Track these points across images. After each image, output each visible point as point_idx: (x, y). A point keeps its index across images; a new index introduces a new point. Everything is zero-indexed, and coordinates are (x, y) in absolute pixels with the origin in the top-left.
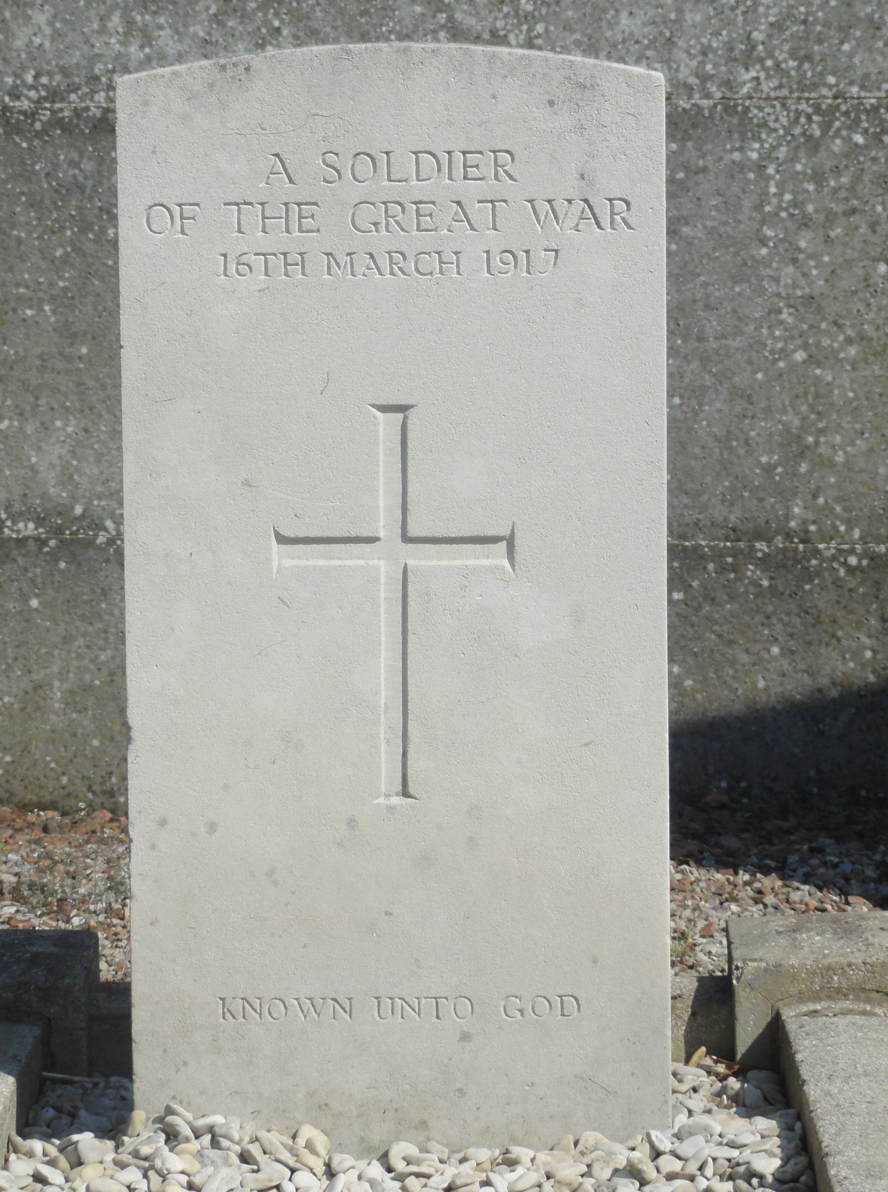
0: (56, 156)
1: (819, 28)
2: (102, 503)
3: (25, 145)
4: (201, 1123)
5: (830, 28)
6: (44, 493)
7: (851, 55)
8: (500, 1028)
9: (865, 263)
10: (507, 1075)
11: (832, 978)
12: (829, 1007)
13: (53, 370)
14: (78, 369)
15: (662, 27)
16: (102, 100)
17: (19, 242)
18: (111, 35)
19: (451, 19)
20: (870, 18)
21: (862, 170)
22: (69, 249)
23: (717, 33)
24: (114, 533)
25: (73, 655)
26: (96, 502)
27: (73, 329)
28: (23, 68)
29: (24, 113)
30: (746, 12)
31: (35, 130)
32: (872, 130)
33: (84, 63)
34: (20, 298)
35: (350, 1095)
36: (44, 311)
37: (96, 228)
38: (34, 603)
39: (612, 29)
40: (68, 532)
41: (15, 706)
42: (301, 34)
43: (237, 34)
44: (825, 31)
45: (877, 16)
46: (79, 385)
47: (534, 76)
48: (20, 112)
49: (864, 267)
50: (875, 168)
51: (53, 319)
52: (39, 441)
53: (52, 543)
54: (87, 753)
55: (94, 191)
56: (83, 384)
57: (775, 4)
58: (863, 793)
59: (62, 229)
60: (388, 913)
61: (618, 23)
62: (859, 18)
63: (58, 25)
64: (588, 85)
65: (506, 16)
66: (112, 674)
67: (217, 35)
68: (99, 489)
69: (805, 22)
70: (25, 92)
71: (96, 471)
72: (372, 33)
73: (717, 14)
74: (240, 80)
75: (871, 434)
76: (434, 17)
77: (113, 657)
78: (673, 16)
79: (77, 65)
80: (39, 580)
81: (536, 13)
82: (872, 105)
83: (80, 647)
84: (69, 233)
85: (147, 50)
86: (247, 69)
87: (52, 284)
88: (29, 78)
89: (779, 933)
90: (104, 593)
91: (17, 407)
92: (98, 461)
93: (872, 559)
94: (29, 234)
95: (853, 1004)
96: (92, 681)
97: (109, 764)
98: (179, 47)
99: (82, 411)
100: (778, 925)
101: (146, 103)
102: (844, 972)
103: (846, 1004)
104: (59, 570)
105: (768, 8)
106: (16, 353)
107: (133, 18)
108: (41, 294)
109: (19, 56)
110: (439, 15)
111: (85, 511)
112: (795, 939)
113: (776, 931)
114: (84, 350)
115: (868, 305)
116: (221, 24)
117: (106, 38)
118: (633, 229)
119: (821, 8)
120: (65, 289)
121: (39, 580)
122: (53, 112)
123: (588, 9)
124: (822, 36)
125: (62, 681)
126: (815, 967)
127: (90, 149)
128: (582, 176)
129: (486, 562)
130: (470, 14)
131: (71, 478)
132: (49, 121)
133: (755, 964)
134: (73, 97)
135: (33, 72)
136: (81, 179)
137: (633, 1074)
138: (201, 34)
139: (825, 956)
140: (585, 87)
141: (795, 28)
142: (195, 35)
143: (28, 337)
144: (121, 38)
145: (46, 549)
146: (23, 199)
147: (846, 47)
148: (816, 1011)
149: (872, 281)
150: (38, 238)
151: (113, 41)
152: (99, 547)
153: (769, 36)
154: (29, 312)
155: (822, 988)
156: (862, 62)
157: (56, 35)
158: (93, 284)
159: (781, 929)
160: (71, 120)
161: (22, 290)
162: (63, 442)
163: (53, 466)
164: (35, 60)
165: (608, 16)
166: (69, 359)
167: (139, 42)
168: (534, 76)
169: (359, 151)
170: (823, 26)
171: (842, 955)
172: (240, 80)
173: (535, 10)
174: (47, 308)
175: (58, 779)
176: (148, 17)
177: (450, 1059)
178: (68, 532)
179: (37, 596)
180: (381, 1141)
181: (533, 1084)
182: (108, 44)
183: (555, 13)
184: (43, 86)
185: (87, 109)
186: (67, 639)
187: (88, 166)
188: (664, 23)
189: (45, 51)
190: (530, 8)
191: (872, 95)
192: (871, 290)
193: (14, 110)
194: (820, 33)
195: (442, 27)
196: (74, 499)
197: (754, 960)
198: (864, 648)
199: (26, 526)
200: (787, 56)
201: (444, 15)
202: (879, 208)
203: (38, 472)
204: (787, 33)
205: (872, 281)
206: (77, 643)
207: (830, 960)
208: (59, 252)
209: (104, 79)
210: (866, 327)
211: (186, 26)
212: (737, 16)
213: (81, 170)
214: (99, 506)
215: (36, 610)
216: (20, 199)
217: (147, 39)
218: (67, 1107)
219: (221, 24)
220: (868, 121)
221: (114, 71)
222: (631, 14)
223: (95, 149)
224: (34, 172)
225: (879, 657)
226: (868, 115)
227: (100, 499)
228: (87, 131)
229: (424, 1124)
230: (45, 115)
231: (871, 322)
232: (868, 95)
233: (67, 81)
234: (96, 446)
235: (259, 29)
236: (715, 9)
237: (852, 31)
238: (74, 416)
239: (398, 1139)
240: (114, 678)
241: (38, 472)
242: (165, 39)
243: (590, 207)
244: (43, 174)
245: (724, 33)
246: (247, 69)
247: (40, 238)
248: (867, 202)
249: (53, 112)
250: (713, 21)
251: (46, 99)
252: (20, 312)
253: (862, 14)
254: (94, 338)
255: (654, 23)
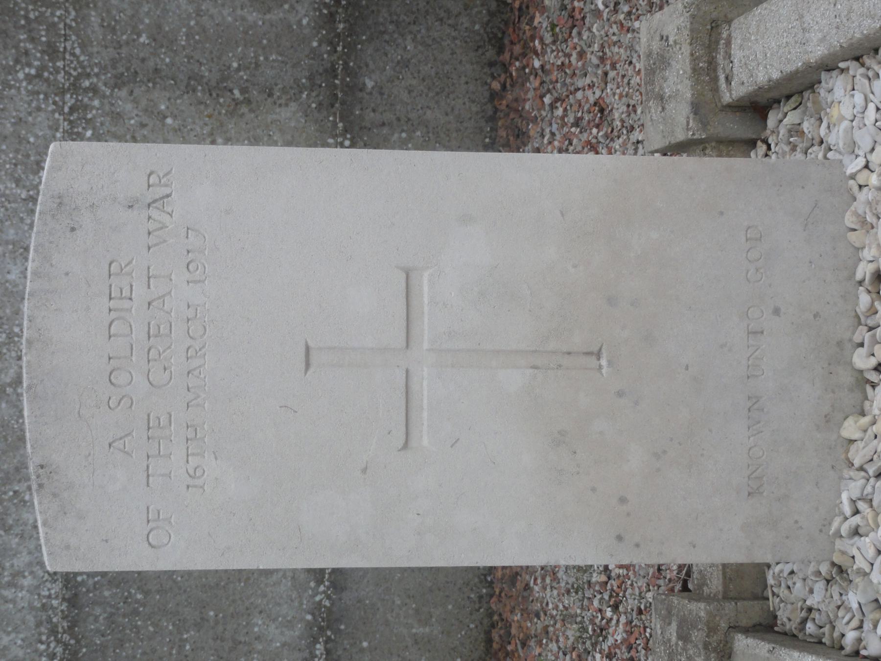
0: (92, 630)
1: (20, 157)
2: (305, 602)
3: (84, 650)
4: (847, 509)
5: (20, 150)
6: (299, 638)
7: (37, 137)
8: (770, 285)
9: (166, 131)
10: (804, 281)
11: (701, 68)
12: (724, 69)
13: (223, 633)
14: (223, 617)
15: (17, 254)
16: (57, 602)
17: (144, 653)
18: (17, 596)
19: (10, 385)
20: (14, 124)
21: (108, 131)
22: (149, 623)
23: (22, 219)
24: (323, 595)
25: (397, 620)
26: (305, 607)
27: (199, 620)
28: (36, 651)
29: (64, 650)
30: (9, 201)
31: (76, 644)
32: (84, 125)
33: (34, 613)
34: (179, 653)
35: (819, 399)
36: (187, 639)
37: (136, 605)
38: (365, 644)
39: (18, 284)
40: (322, 624)
41: (427, 656)
42: (18, 478)
43: (17, 518)
44: (21, 152)
45: (13, 120)
46: (232, 616)
47: (51, 242)
48: (64, 653)
49: (168, 132)
50: (107, 124)
51: (192, 633)
52: (267, 640)
53: (329, 633)
54: (456, 612)
55: (111, 606)
56: (232, 614)
57: (5, 183)
58: (487, 140)
59: (136, 627)
60: (687, 368)
61: (14, 281)
62: (14, 131)
63: (10, 629)
64: (58, 201)
65: (9, 350)
66: (409, 597)
67: (17, 530)
68: (296, 604)
69: (16, 165)
70: (51, 649)
71: (285, 606)
72: (18, 434)
73: (10, 219)
74: (51, 473)
75: (270, 131)
76: (8, 395)
77: (399, 596)
78: (11, 247)
79: (35, 617)
80: (351, 641)
81: (8, 332)
82: (68, 125)
83: (392, 616)
84: (139, 623)
85: (26, 574)
86: (42, 467)
87: (171, 633)
88: (42, 647)
89: (663, 109)
90: (359, 601)
91: (246, 655)
92: (279, 604)
93: (346, 131)
94: (139, 647)
95: (720, 54)
96: (413, 609)
97: (463, 599)
98: (24, 554)
99: (249, 615)
100: (656, 113)
101: (68, 547)
102: (697, 58)
103: (720, 58)
104: (346, 629)
105: (6, 188)
106: (213, 655)
107: (6, 582)
108: (177, 640)
109: (29, 653)
110: (7, 392)
111: (309, 613)
112: (670, 97)
113: (661, 112)
114: (212, 613)
115: (191, 130)
116: (11, 527)
117: (18, 600)
118: (172, 169)
119: (7, 155)
120: (173, 625)
121: (351, 641)
122: (64, 632)
123: (5, 299)
124: (25, 154)
125: (412, 627)
126: (694, 79)
127: (87, 609)
128: (130, 207)
129: (426, 289)
130: (7, 372)
131: (288, 621)
132: (69, 635)
133: (691, 121)
134: (55, 620)
135: (39, 645)
136: (105, 615)
137: (803, 188)
138: (17, 540)
139: (685, 72)
140: (60, 203)
141: (20, 171)
142: (18, 544)
143: (203, 648)
144: (19, 590)
145: (333, 637)
146: (118, 651)
147: (32, 140)
148: (727, 78)
149: (177, 127)
150: (142, 642)
151: (20, 595)
152: (332, 604)
153: (24, 187)
154: (188, 647)
155: (708, 75)
156: (41, 130)
157: (16, 630)
158: (171, 608)
159: (660, 109)
160: (68, 622)
161: (174, 652)
162: (267, 626)
163: (282, 633)
164: (31, 643)
165: (10, 287)
166: (217, 623)
167: (21, 578)
168: (51, 242)
169: (108, 380)
170: (18, 153)
171: (684, 61)
172: (51, 473)
173: (5, 333)
174: (185, 636)
175: (471, 630)
176: (6, 574)
177: (793, 323)
178: (322, 624)
179: (361, 642)
180: (852, 376)
181: (811, 262)
182: (22, 598)
183: (8, 320)
184: (48, 638)
185: (62, 611)
186: (387, 623)
187: (98, 611)
188: (15, 252)
189: (26, 637)
190: (4, 335)
191: (62, 124)
192: (182, 128)
193: (62, 656)
194: (23, 155)
195: (15, 389)
196: (302, 619)
197: (688, 123)
198: (400, 137)
199: (319, 649)
200: (37, 177)
201: (8, 389)
202: (132, 122)
203: (286, 642)
204: (22, 176)
205: (177, 127)
206: (390, 618)
207: (689, 69)
208: (151, 629)
209: (44, 601)
210: (205, 132)
211: (11, 549)
212: (11, 207)
213: (100, 615)
214: (306, 604)
215: (369, 643)
216: (117, 653)
217: (18, 574)
218: (804, 614)
219: (11, 527)
220: (78, 127)
221: (39, 595)
222: (8, 273)
223: (88, 606)
224: (101, 645)
225: (405, 128)
226: (74, 127)
227: (302, 604)
228: (76, 611)
229: (840, 344)
230: (66, 637)
231: (202, 128)
232: (62, 127)
233: (45, 623)
234: (271, 606)
235: (14, 504)
236: (6, 220)
237: (22, 136)
238: (252, 619)
239: (851, 363)
240: (411, 595)
241: (286, 642)
242: (22, 560)
243: (155, 201)
244: (102, 639)
245: (21, 215)
246: (42, 467)
247: (142, 640)
248: (128, 129)
249: (64, 632)
250: (14, 222)
251: (56, 637)
252: (187, 653)
253: (11, 130)
254: (204, 607)
255: (14, 258)
